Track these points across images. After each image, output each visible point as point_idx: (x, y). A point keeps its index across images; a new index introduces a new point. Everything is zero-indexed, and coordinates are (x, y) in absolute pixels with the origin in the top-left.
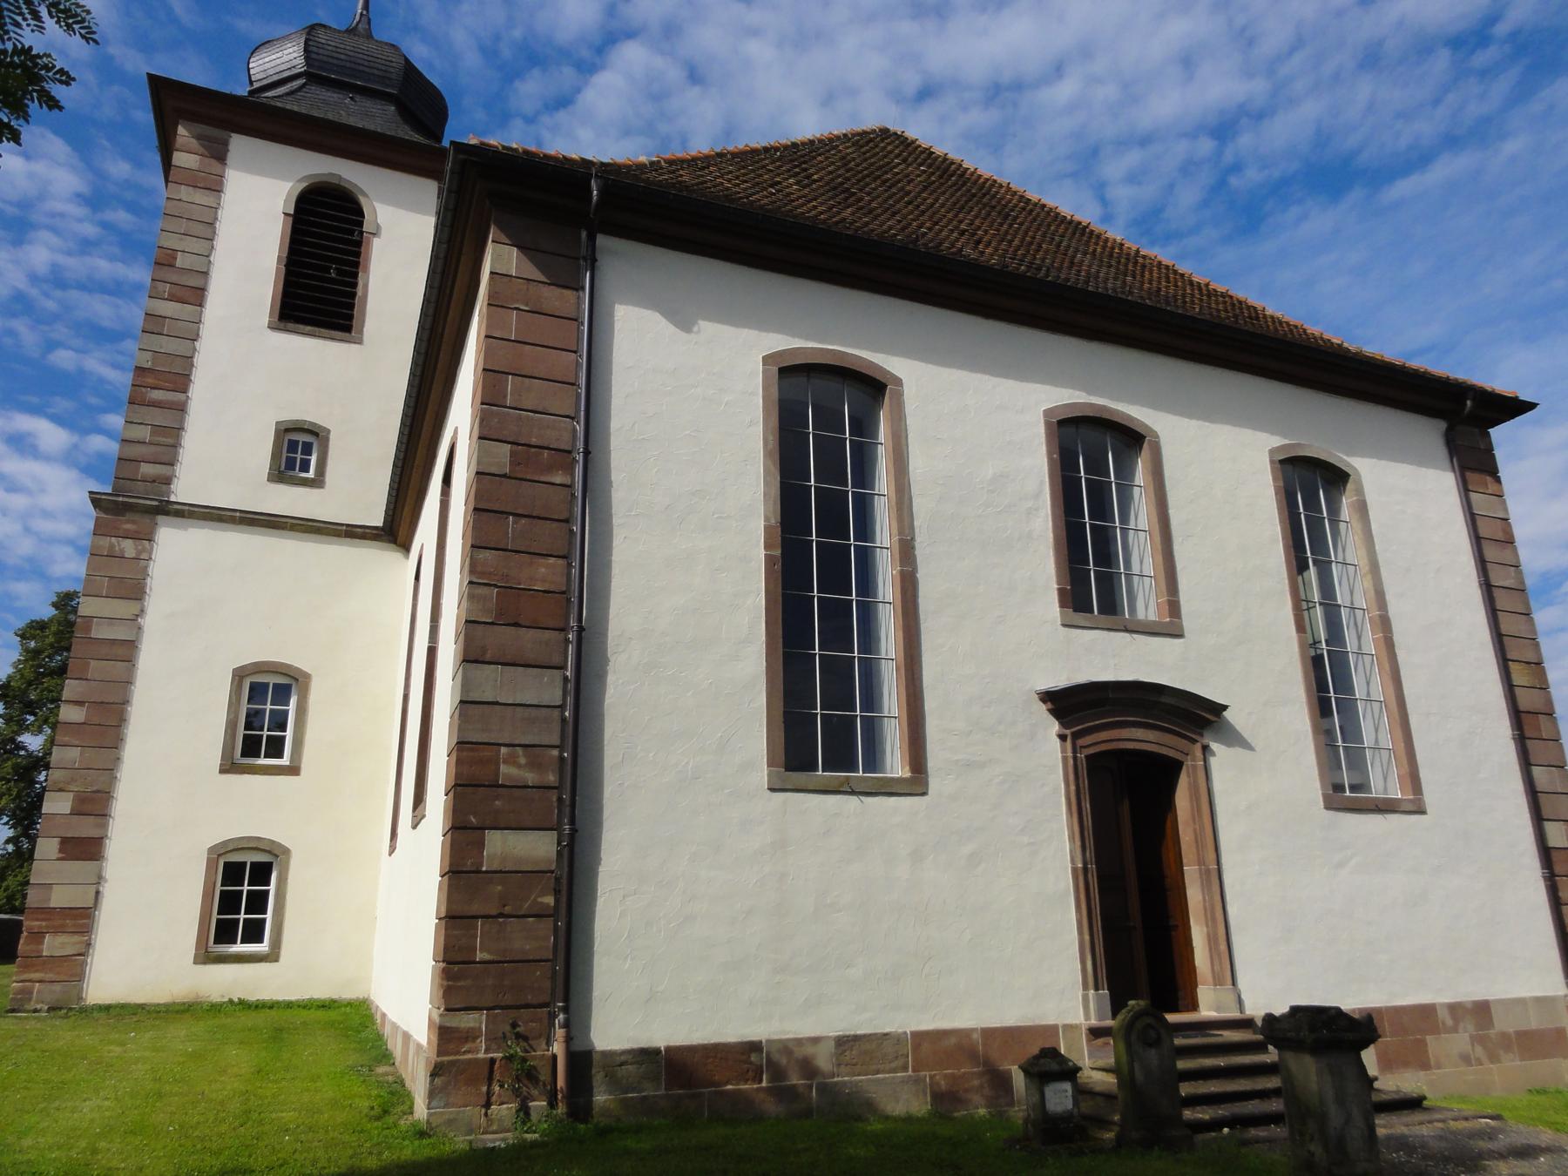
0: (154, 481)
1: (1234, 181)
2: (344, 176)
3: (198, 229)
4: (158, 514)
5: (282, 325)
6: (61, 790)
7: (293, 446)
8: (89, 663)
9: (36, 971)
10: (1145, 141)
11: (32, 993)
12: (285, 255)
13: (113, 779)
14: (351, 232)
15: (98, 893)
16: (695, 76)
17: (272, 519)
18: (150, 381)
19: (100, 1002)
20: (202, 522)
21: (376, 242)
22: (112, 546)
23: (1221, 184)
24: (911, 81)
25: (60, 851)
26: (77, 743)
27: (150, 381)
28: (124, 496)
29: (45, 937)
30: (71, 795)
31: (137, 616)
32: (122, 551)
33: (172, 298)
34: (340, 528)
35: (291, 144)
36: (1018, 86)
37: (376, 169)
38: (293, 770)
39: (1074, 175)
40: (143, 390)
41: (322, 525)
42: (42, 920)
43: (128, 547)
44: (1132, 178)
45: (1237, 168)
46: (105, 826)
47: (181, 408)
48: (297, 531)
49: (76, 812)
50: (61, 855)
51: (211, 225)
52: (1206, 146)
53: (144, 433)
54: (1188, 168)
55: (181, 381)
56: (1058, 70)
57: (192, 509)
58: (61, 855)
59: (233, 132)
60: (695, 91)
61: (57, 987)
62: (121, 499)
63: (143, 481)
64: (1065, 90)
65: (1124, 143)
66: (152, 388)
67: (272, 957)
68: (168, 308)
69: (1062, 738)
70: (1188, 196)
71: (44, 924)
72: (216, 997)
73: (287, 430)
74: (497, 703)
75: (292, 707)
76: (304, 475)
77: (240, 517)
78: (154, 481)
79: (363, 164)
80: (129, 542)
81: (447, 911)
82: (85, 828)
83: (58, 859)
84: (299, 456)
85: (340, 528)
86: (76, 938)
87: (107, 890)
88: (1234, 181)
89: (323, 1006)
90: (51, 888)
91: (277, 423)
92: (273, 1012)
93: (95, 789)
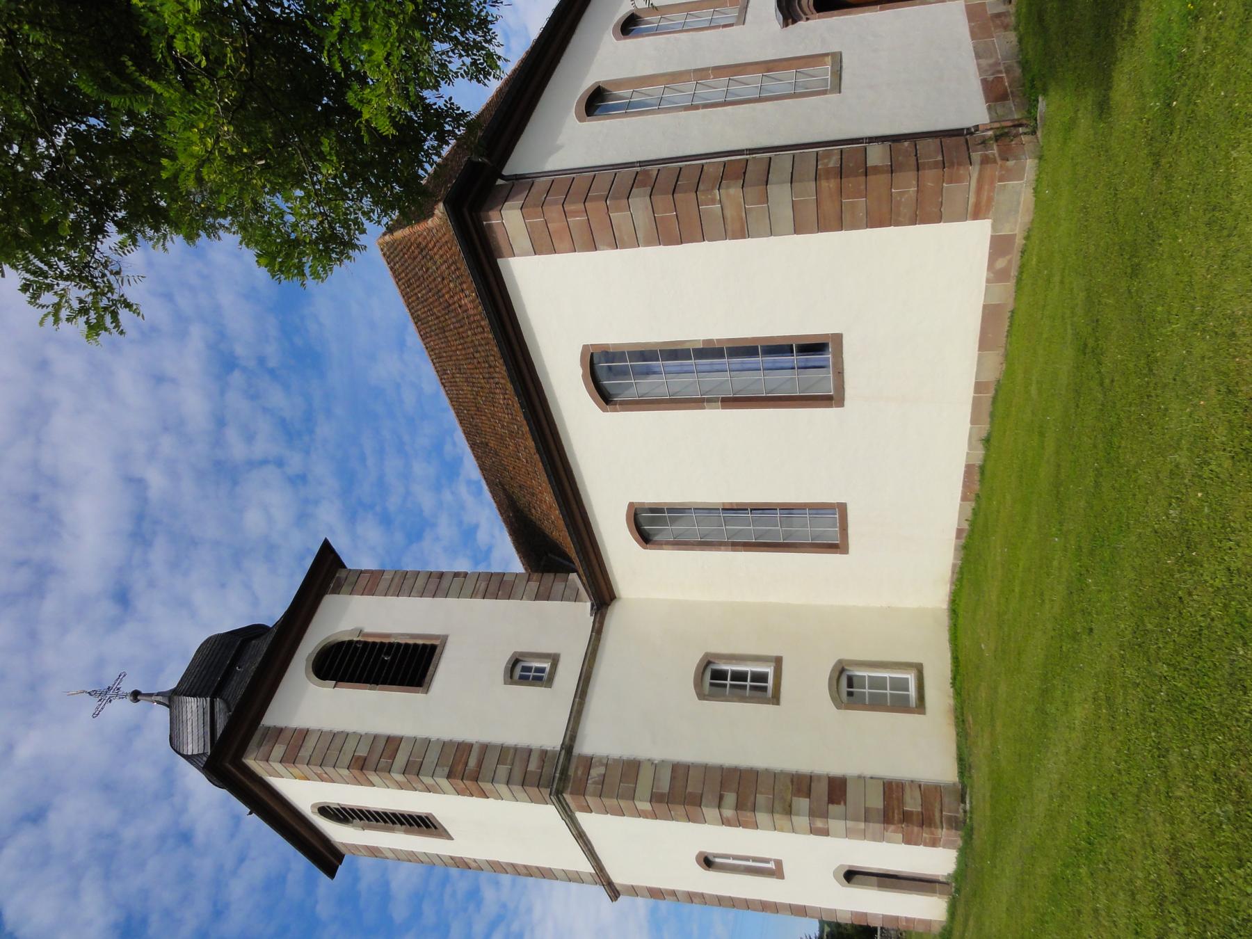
0: (543, 761)
1: (272, 363)
2: (310, 652)
3: (338, 742)
4: (571, 753)
5: (425, 685)
6: (790, 806)
7: (522, 677)
8: (690, 793)
9: (934, 815)
10: (221, 422)
11: (951, 816)
12: (369, 685)
13: (783, 774)
14: (356, 648)
15: (872, 778)
16: (36, 817)
17: (583, 678)
18: (460, 768)
19: (956, 772)
20: (581, 725)
21: (368, 630)
22: (595, 783)
23: (272, 372)
24: (108, 608)
25: (839, 803)
26: (752, 798)
27: (460, 768)
28: (555, 773)
29: (907, 811)
30: (795, 799)
31: (652, 763)
32: (599, 775)
33: (393, 757)
34: (593, 637)
35: (283, 675)
36: (139, 517)
37: (287, 675)
38: (778, 662)
39: (235, 483)
40: (467, 771)
41: (590, 648)
42: (893, 813)
43: (596, 772)
44: (250, 438)
45: (262, 361)
46: (819, 777)
47: (485, 748)
48: (593, 665)
49: (809, 795)
50: (842, 803)
51: (335, 735)
52: (237, 378)
53: (503, 770)
54: (253, 396)
55: (463, 749)
56: (136, 484)
57: (570, 729)
58: (842, 803)
59: (259, 723)
60: (53, 818)
61: (946, 800)
62: (557, 775)
63: (543, 767)
64: (156, 480)
65: (218, 441)
66: (466, 766)
67: (919, 669)
68: (401, 759)
69: (808, 19)
70: (277, 398)
71: (896, 811)
72: (950, 702)
73: (511, 677)
74: (792, 173)
75: (729, 667)
76: (547, 670)
77: (580, 697)
78: (543, 761)
79: (303, 641)
80: (592, 771)
81: (878, 822)
82: (821, 790)
83: (845, 804)
84: (532, 674)
85: (593, 637)
86: (908, 790)
87: (868, 772)
88: (272, 363)
89: (955, 625)
90: (868, 808)
91: (505, 684)
92: (961, 612)
93: (790, 784)
